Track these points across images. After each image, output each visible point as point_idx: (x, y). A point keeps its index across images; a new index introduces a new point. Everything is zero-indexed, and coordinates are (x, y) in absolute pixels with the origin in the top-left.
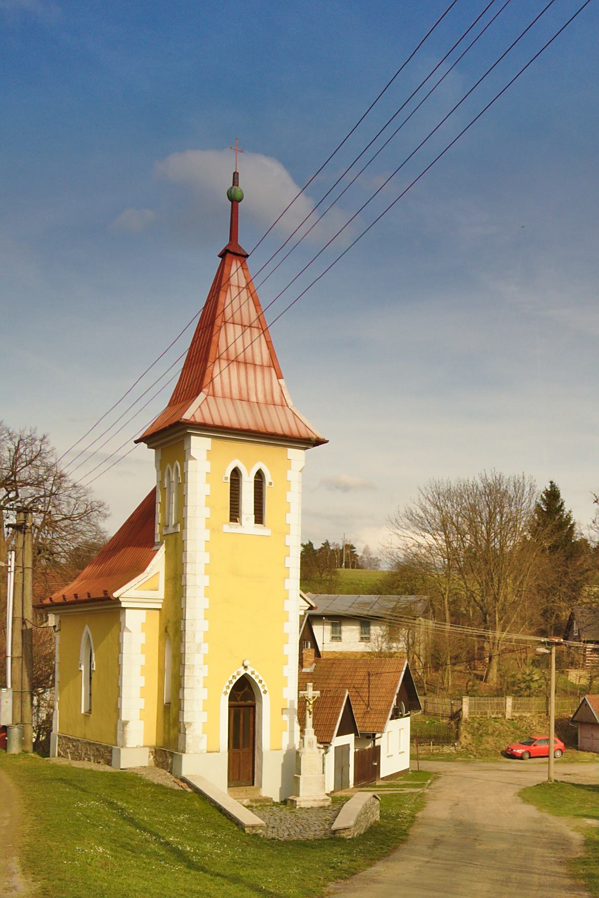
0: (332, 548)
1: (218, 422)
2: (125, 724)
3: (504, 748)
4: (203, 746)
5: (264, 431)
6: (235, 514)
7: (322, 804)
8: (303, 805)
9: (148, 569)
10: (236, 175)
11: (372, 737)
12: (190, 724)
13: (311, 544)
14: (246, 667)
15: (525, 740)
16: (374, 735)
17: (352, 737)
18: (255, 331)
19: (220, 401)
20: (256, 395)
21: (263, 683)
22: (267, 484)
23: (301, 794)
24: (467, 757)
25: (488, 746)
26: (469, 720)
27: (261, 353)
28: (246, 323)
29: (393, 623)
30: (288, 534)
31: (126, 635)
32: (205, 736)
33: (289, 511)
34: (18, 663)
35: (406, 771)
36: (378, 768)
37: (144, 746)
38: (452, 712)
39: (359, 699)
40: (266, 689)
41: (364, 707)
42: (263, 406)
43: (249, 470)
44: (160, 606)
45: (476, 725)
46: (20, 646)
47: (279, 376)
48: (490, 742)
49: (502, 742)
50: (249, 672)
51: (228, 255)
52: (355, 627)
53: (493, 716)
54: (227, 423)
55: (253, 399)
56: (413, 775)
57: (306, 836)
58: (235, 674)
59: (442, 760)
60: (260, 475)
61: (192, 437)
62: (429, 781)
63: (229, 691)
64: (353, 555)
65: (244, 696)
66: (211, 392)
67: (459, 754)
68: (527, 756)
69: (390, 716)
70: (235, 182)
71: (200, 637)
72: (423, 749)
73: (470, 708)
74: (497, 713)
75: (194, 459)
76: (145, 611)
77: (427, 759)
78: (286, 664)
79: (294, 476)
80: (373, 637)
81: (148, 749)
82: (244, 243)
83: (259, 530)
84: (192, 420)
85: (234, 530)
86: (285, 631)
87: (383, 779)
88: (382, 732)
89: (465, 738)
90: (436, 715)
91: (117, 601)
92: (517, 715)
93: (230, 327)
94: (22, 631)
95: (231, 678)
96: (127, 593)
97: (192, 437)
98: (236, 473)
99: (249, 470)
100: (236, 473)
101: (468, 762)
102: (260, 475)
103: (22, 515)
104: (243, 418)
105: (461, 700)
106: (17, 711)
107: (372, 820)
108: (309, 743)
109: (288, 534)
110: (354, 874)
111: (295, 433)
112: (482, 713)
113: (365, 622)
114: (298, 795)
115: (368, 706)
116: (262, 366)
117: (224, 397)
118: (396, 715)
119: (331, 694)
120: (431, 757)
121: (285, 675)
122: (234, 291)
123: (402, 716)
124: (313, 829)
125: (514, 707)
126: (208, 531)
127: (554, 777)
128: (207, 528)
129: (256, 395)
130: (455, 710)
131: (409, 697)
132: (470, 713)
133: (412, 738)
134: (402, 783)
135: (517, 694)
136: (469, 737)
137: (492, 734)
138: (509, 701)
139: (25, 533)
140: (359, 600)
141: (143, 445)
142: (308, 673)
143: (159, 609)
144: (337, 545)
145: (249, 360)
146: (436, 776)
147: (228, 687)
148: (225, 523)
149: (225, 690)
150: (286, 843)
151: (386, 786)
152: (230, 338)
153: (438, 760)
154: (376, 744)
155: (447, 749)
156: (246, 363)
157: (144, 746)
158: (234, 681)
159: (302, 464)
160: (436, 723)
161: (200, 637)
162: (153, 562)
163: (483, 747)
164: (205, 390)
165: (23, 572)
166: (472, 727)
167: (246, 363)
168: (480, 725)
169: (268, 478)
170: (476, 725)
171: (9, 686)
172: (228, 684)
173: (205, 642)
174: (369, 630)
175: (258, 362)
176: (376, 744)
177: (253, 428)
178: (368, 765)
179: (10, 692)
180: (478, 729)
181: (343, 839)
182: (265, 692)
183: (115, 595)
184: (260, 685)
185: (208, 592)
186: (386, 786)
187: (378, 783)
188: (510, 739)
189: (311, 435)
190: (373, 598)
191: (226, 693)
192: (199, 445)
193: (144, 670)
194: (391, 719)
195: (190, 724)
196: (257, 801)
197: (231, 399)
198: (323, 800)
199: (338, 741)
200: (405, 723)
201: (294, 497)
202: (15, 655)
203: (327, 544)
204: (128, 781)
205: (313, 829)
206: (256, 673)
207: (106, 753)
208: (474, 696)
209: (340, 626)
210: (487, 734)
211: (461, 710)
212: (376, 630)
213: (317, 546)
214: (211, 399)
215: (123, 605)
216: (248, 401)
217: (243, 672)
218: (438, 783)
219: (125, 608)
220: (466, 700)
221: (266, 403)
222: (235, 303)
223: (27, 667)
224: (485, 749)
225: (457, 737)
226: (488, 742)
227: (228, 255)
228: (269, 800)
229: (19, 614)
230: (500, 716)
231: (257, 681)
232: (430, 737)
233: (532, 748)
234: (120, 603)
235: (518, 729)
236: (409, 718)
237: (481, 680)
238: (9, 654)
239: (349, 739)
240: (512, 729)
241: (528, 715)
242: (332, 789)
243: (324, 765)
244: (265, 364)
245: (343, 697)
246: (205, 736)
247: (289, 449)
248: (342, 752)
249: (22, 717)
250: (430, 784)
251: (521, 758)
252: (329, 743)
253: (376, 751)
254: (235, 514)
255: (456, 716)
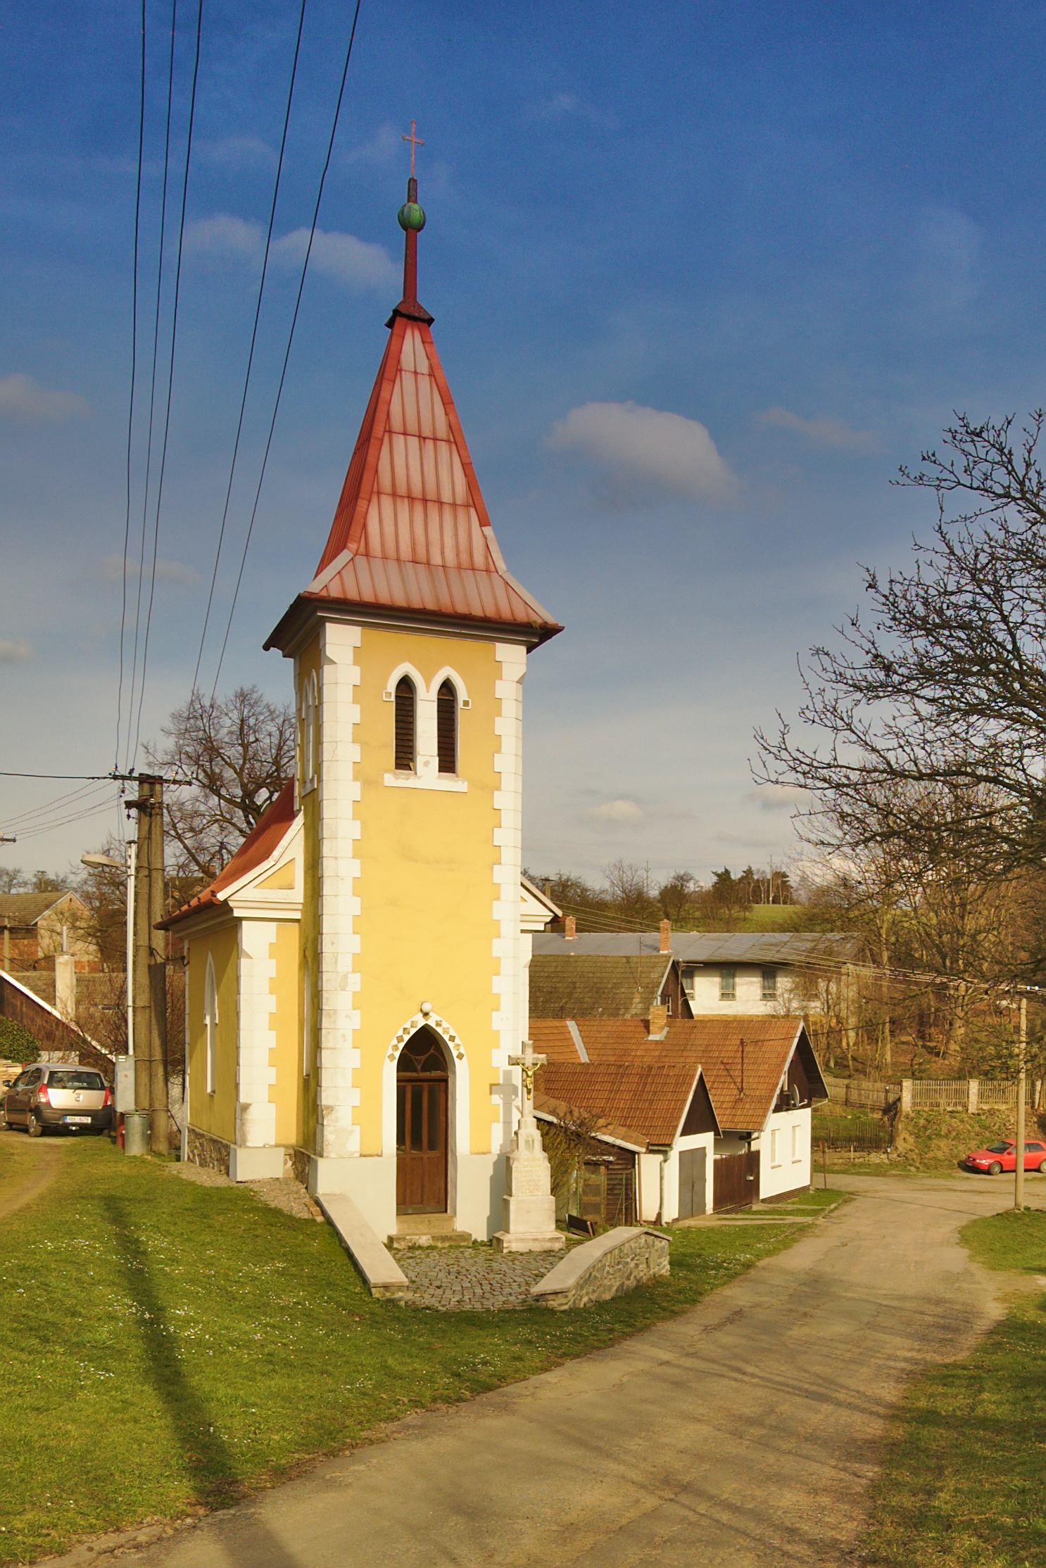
0: (756, 877)
1: (368, 597)
2: (245, 1108)
3: (964, 1157)
4: (354, 1145)
5: (450, 611)
6: (405, 757)
7: (548, 1246)
8: (515, 1247)
9: (276, 853)
10: (412, 182)
11: (747, 1137)
12: (331, 1108)
13: (727, 872)
14: (426, 1014)
15: (996, 1145)
16: (749, 1135)
17: (710, 1136)
18: (443, 447)
19: (377, 564)
20: (442, 553)
21: (457, 1041)
22: (460, 704)
23: (512, 1228)
24: (905, 1169)
25: (940, 1155)
26: (913, 1115)
27: (453, 484)
28: (427, 432)
29: (808, 973)
30: (499, 789)
31: (244, 962)
32: (358, 1128)
33: (499, 751)
34: (143, 1017)
35: (804, 1189)
36: (756, 1184)
37: (277, 1146)
38: (887, 1102)
39: (729, 1079)
40: (462, 1051)
41: (736, 1092)
42: (453, 575)
43: (428, 682)
44: (298, 915)
45: (922, 1122)
46: (147, 991)
47: (484, 522)
48: (942, 1149)
49: (961, 1147)
50: (431, 1022)
51: (398, 319)
52: (755, 979)
53: (949, 1109)
54: (384, 598)
55: (437, 560)
56: (815, 1200)
57: (488, 1304)
58: (408, 1025)
59: (866, 1174)
60: (447, 689)
61: (328, 625)
62: (832, 1206)
63: (397, 1054)
64: (785, 885)
65: (424, 1063)
66: (362, 549)
67: (894, 1165)
68: (997, 1169)
69: (772, 1107)
70: (412, 197)
71: (345, 964)
72: (833, 1157)
73: (914, 1097)
74: (955, 1104)
75: (333, 662)
76: (530, 935)
77: (843, 1172)
78: (497, 1009)
79: (507, 690)
80: (778, 993)
81: (282, 1151)
82: (426, 301)
83: (447, 783)
84: (324, 593)
85: (402, 782)
86: (495, 954)
87: (764, 1201)
88: (760, 1130)
89: (905, 1141)
90: (862, 1106)
91: (225, 907)
92: (986, 1107)
93: (399, 441)
94: (150, 966)
95: (400, 1033)
96: (242, 894)
97: (328, 625)
98: (406, 685)
99: (428, 682)
100: (406, 685)
101: (907, 1176)
102: (447, 689)
103: (146, 786)
104: (420, 593)
105: (900, 1084)
106: (142, 1090)
107: (643, 1273)
108: (527, 1142)
109: (499, 789)
110: (488, 1388)
111: (506, 614)
112: (931, 1104)
113: (768, 970)
114: (507, 1231)
115: (741, 1090)
116: (454, 505)
117: (385, 557)
118: (785, 1104)
119: (676, 1071)
120: (850, 1169)
121: (495, 1027)
122: (408, 379)
123: (795, 1107)
124: (507, 1290)
125: (981, 1095)
126: (358, 784)
127: (1023, 1203)
128: (355, 779)
129: (442, 553)
130: (891, 1098)
131: (806, 1082)
132: (914, 1104)
133: (816, 1141)
134: (790, 1207)
135: (987, 1076)
136: (911, 1139)
137: (946, 1136)
138: (974, 1086)
139: (151, 815)
140: (764, 939)
141: (275, 652)
142: (657, 1042)
143: (298, 921)
144: (764, 872)
145: (431, 495)
146: (847, 1197)
147: (396, 1047)
148: (386, 771)
149: (390, 1052)
150: (447, 1316)
151: (766, 1213)
152: (402, 460)
153: (859, 1174)
154: (753, 1149)
155: (876, 1158)
156: (425, 501)
157: (277, 1146)
158: (407, 1038)
159: (521, 670)
160: (863, 1118)
161: (345, 964)
162: (284, 842)
163: (931, 1155)
164: (353, 546)
165: (149, 876)
166: (916, 1125)
167: (425, 501)
168: (929, 1122)
169: (462, 694)
170: (922, 1122)
171: (131, 1051)
172: (395, 1042)
173: (354, 972)
174: (775, 983)
175: (446, 497)
176: (753, 1149)
177: (431, 605)
178: (739, 1179)
179: (131, 1061)
180: (925, 1128)
181: (552, 1312)
182: (460, 1056)
183: (221, 896)
184: (451, 1044)
185: (359, 886)
186: (766, 1213)
187: (755, 1208)
188: (973, 1144)
189: (534, 618)
190: (785, 937)
191: (391, 1057)
192: (340, 639)
193: (275, 1021)
194: (775, 1111)
195: (331, 1108)
196: (444, 1239)
197: (398, 560)
198: (551, 1240)
199: (683, 1143)
200: (802, 1118)
201: (508, 726)
202: (140, 1003)
203: (749, 872)
204: (243, 1200)
205: (507, 1290)
206: (445, 1024)
207: (220, 1152)
208: (921, 1079)
209: (734, 976)
210: (939, 1135)
211: (899, 1099)
212: (784, 983)
213: (736, 875)
214: (361, 561)
215: (237, 913)
216: (428, 563)
217: (421, 1022)
218: (846, 1209)
219: (240, 919)
220: (907, 1084)
221: (459, 567)
222: (413, 399)
223: (158, 1021)
224: (935, 1158)
225: (891, 1141)
226: (939, 1148)
227: (398, 319)
228: (465, 1237)
229: (144, 941)
230: (960, 1108)
231: (446, 1038)
232: (849, 1140)
233: (1006, 1156)
234: (231, 910)
235: (986, 1128)
236: (809, 1110)
237: (937, 1054)
238: (130, 1003)
239: (705, 1140)
240: (977, 1129)
241: (1003, 1107)
242: (676, 1216)
243: (661, 1178)
244: (458, 502)
245: (693, 1076)
246: (358, 1128)
247: (498, 645)
248: (692, 1160)
249: (151, 1099)
250: (832, 1211)
251: (988, 1172)
252: (669, 1145)
253: (754, 1158)
254: (405, 757)
255: (892, 1109)
